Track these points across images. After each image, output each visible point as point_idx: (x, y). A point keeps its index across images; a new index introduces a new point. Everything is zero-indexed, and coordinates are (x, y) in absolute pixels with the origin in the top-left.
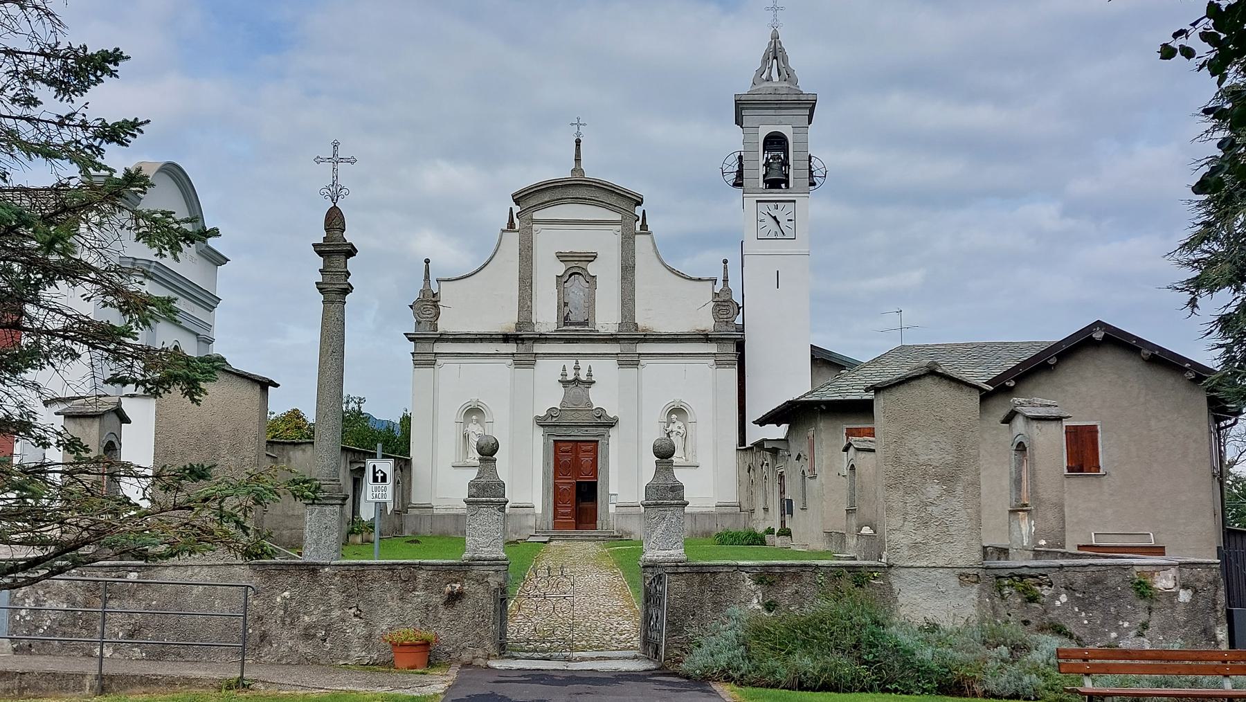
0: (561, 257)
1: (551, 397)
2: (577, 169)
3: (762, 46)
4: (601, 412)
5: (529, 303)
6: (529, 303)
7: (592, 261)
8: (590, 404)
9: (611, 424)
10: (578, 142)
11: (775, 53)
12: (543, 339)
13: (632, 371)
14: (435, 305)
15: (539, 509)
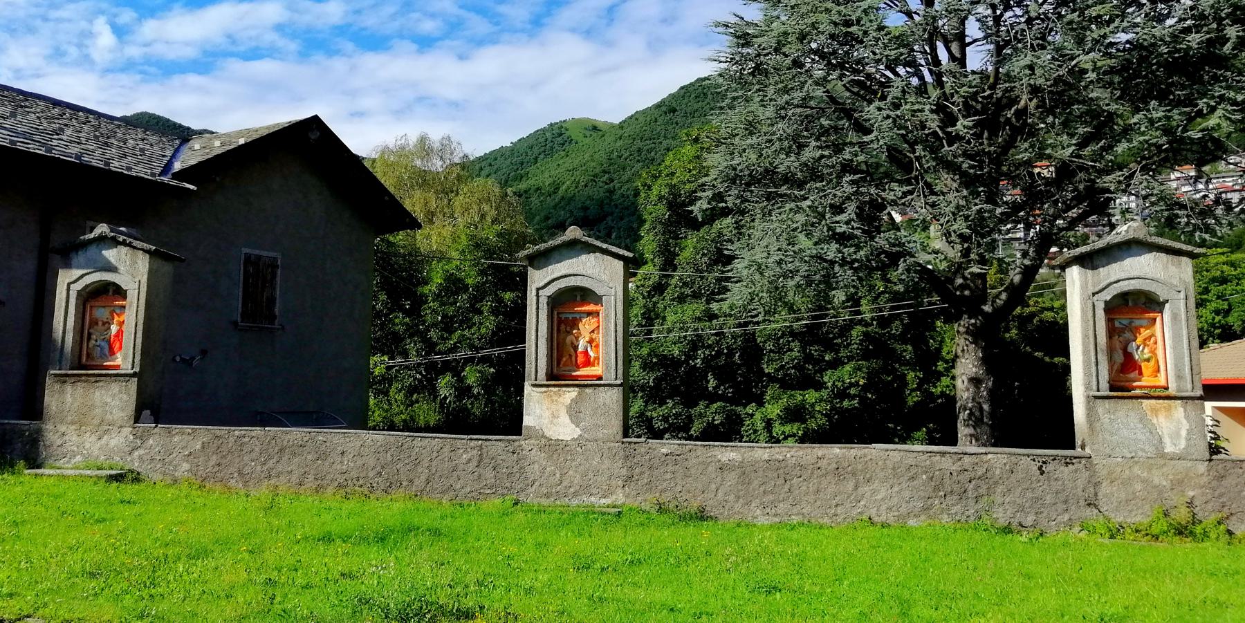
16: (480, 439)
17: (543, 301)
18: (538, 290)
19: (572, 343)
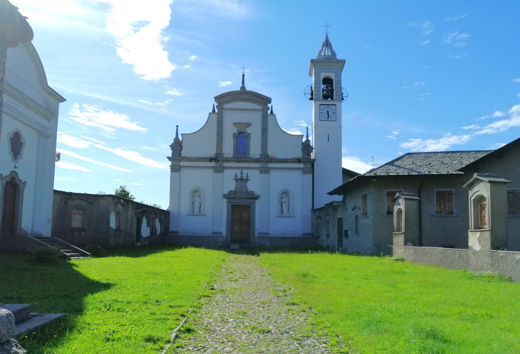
0: (236, 124)
1: (230, 186)
2: (243, 88)
3: (323, 40)
4: (252, 193)
5: (221, 145)
6: (221, 145)
7: (249, 127)
8: (247, 189)
9: (257, 198)
10: (243, 76)
11: (327, 44)
12: (228, 160)
13: (266, 175)
14: (181, 146)
15: (224, 234)
16: (460, 250)
17: (472, 201)
18: (471, 198)
19: (484, 216)
